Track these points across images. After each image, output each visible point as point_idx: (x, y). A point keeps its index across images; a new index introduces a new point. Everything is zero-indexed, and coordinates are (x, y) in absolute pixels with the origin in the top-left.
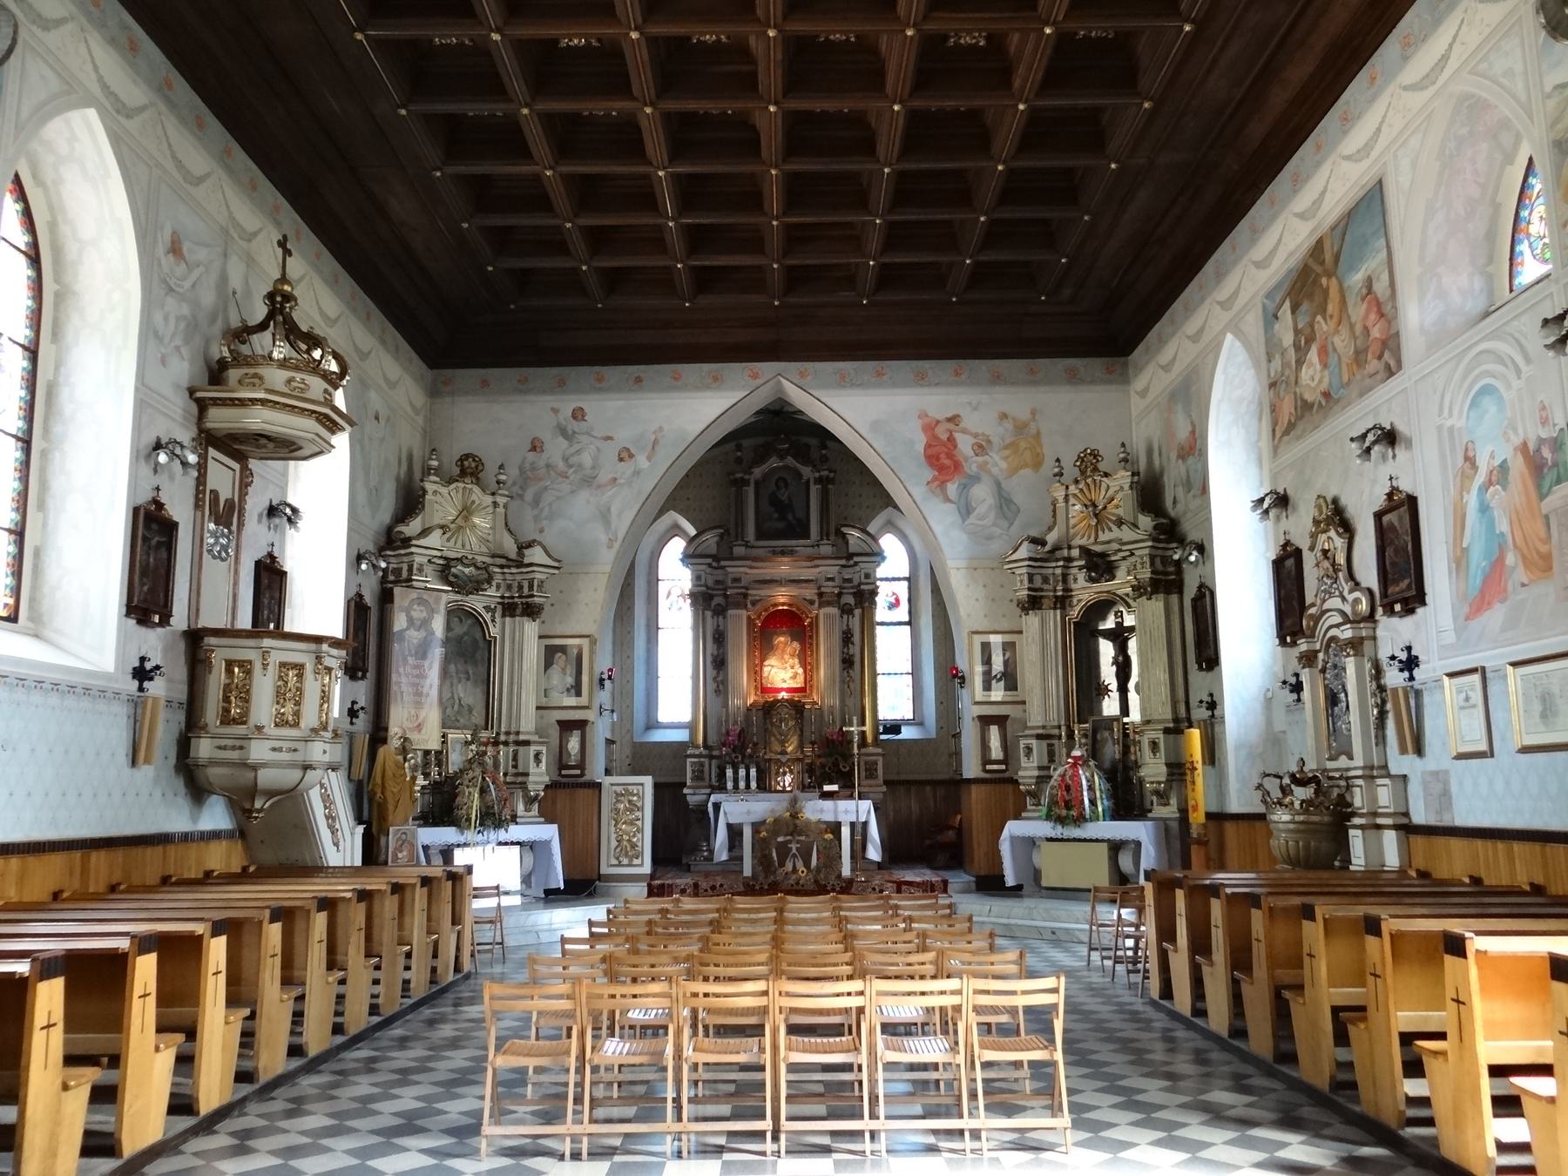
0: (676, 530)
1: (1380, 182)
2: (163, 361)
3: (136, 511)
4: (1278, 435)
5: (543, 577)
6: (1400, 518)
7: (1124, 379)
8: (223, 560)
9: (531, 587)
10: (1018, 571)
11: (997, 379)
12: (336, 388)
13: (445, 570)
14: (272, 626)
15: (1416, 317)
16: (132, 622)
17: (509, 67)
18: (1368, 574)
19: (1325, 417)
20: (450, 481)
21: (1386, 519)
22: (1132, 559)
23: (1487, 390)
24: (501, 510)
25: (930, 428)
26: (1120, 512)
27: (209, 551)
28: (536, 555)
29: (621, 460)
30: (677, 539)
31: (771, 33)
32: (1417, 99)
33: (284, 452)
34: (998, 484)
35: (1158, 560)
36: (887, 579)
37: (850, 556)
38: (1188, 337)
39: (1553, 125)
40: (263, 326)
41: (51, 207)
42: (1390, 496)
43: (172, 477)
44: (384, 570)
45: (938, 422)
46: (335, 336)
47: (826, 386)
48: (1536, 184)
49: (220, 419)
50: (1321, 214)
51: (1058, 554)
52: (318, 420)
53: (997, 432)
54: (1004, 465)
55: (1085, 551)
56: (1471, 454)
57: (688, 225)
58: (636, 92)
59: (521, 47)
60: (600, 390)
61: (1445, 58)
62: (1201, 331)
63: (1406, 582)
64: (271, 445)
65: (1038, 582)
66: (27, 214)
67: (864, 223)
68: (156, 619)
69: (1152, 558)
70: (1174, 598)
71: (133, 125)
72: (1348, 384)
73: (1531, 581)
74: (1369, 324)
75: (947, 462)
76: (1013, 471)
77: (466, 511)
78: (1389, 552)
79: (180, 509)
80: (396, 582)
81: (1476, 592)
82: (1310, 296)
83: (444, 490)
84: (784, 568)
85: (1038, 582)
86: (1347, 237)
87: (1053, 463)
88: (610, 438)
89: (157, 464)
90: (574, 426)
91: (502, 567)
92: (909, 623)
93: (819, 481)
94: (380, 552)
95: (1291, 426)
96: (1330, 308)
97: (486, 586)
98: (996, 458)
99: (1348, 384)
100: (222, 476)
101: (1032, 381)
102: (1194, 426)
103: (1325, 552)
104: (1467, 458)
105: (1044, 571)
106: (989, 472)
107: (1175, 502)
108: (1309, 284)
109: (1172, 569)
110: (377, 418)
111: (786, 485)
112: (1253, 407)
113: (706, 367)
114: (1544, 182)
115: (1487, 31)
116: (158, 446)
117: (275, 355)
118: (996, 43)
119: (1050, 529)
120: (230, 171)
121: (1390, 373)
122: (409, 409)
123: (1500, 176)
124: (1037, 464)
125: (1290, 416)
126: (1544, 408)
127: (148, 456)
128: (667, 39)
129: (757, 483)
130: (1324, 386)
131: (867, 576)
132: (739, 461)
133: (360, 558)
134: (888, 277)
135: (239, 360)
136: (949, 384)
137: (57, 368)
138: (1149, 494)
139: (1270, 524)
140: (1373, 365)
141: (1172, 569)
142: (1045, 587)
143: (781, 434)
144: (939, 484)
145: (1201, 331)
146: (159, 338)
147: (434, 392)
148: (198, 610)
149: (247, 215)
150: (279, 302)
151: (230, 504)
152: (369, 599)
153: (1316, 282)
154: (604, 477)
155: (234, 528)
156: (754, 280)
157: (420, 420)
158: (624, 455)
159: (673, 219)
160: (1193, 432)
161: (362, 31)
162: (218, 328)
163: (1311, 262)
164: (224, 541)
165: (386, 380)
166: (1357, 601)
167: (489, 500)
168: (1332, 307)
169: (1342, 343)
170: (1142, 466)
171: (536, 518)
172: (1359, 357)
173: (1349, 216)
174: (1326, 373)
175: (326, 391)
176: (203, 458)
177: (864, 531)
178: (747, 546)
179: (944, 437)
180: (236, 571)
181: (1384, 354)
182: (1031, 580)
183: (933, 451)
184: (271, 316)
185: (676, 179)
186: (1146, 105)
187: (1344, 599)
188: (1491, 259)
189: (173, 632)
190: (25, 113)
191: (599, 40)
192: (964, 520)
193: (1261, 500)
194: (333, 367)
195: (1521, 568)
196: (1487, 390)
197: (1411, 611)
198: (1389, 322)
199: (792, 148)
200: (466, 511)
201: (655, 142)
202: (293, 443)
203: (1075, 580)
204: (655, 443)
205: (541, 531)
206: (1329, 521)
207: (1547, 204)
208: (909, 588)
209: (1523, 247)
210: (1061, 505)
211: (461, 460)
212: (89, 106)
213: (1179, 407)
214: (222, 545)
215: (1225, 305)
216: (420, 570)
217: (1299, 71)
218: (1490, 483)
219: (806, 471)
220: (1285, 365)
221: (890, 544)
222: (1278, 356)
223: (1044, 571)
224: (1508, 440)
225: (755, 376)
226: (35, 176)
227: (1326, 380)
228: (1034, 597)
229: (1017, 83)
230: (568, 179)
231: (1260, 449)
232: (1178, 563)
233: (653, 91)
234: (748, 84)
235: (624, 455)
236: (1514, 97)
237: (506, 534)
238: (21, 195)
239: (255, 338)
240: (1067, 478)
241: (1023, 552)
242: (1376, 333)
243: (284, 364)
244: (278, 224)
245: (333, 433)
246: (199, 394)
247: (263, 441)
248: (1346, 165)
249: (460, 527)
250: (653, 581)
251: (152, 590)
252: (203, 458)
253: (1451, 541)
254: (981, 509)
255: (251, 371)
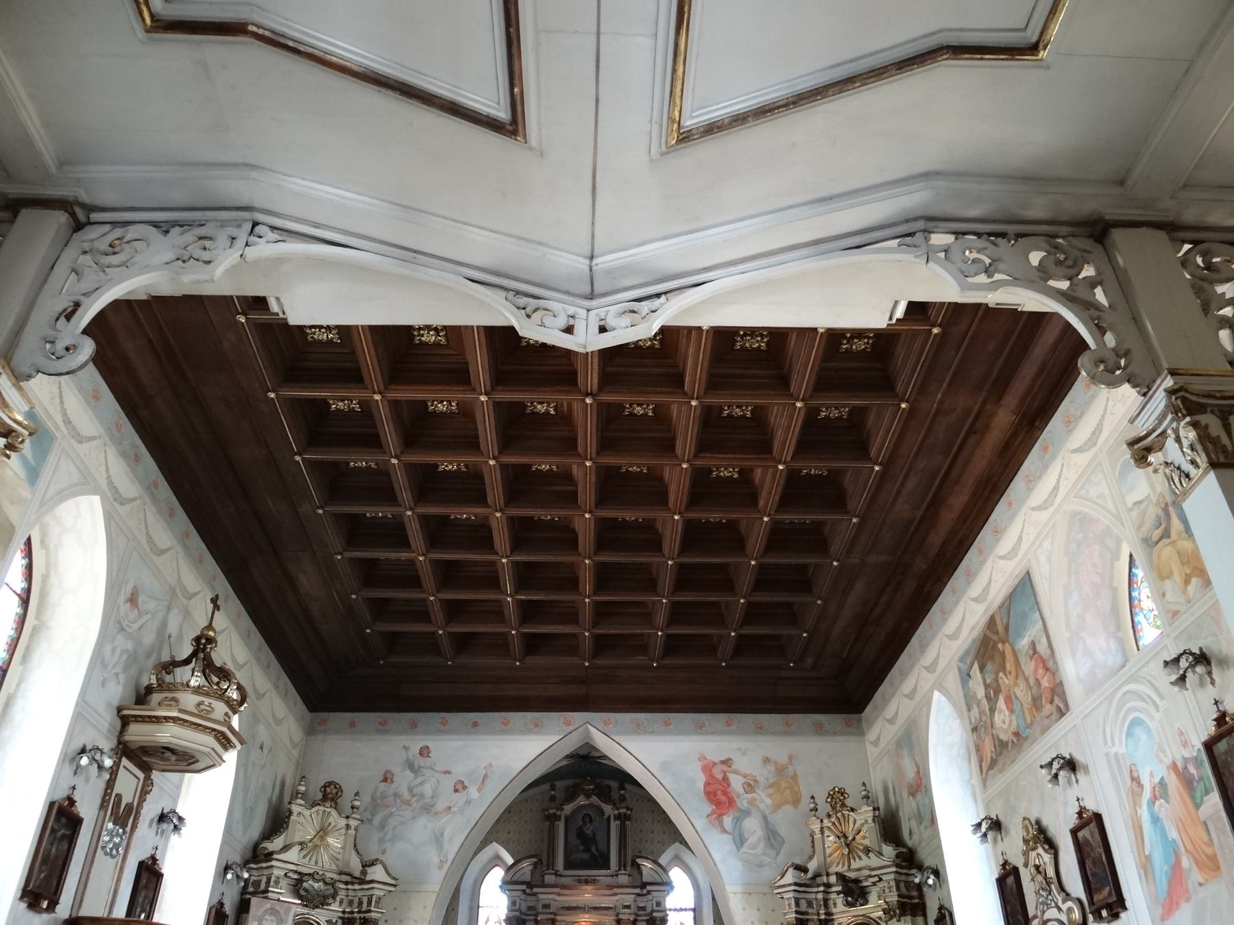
0: (496, 861)
1: (1028, 573)
2: (103, 684)
3: (52, 804)
4: (985, 770)
5: (381, 893)
6: (1092, 834)
7: (861, 733)
8: (113, 857)
9: (369, 903)
10: (786, 896)
11: (760, 730)
12: (235, 713)
13: (297, 888)
14: (143, 916)
15: (1072, 670)
16: (23, 905)
17: (401, 480)
18: (1075, 886)
19: (1019, 752)
20: (314, 805)
21: (1080, 834)
22: (881, 885)
23: (1136, 722)
24: (352, 832)
25: (708, 769)
26: (867, 842)
27: (103, 848)
28: (377, 873)
29: (456, 791)
30: (497, 869)
31: (588, 464)
32: (1044, 516)
33: (182, 766)
34: (765, 818)
35: (902, 885)
36: (675, 910)
37: (643, 885)
38: (905, 696)
39: (1139, 528)
40: (187, 662)
41: (48, 565)
42: (1080, 814)
43: (87, 780)
44: (246, 881)
45: (714, 764)
46: (240, 676)
47: (625, 733)
48: (1139, 573)
49: (138, 734)
50: (990, 597)
51: (819, 880)
52: (216, 738)
53: (763, 774)
54: (769, 801)
55: (841, 877)
56: (1135, 775)
57: (522, 601)
58: (490, 501)
59: (410, 468)
60: (444, 732)
61: (1056, 488)
62: (915, 690)
63: (1107, 889)
64: (173, 758)
65: (804, 907)
66: (29, 568)
67: (654, 602)
68: (45, 904)
69: (897, 882)
70: (920, 920)
71: (123, 510)
72: (1031, 724)
73: (1207, 880)
74: (1039, 677)
75: (723, 798)
76: (777, 807)
77: (323, 832)
78: (1088, 864)
79: (87, 809)
80: (254, 894)
81: (1165, 895)
82: (992, 658)
83: (307, 812)
84: (587, 895)
85: (804, 907)
86: (1012, 613)
87: (808, 800)
88: (449, 772)
89: (78, 766)
90: (421, 761)
91: (346, 883)
92: (694, 910)
93: (618, 817)
94: (245, 864)
95: (993, 763)
96: (1008, 666)
97: (331, 901)
98: (763, 795)
99: (1031, 724)
100: (127, 784)
101: (788, 732)
102: (918, 767)
103: (1037, 867)
104: (1133, 779)
105: (808, 896)
106: (757, 807)
107: (911, 833)
108: (990, 648)
109: (915, 893)
110: (261, 748)
111: (591, 821)
112: (963, 751)
113: (530, 715)
114: (1143, 570)
115: (1080, 470)
116: (83, 751)
117: (193, 683)
118: (745, 475)
119: (811, 858)
120: (185, 547)
121: (1062, 713)
122: (288, 743)
123: (1112, 568)
124: (796, 802)
125: (992, 754)
126: (1182, 733)
127: (73, 760)
128: (514, 466)
129: (567, 818)
130: (1013, 728)
131: (658, 904)
132: (553, 799)
133: (227, 868)
134: (673, 645)
135: (162, 686)
136: (722, 733)
137: (19, 684)
138: (889, 828)
139: (989, 846)
140: (1048, 708)
141: (915, 893)
142: (810, 911)
143: (588, 774)
144: (717, 816)
145: (915, 690)
146: (104, 665)
147: (310, 731)
148: (81, 901)
149: (191, 581)
150: (203, 643)
151: (129, 807)
152: (228, 908)
153: (994, 647)
154: (440, 805)
155: (128, 829)
156: (569, 645)
157: (295, 753)
158: (459, 787)
159: (511, 596)
160: (918, 772)
161: (300, 455)
162: (152, 661)
163: (988, 633)
164: (117, 840)
165: (274, 717)
166: (1070, 910)
167: (343, 822)
168: (1009, 666)
169: (1021, 692)
170: (881, 804)
171: (381, 841)
172: (1036, 703)
173: (1011, 598)
174: (1014, 717)
175: (226, 714)
176: (117, 765)
177: (656, 862)
178: (556, 875)
179: (720, 777)
180: (122, 868)
181: (1053, 700)
182: (797, 904)
183: (711, 788)
184: (194, 654)
185: (516, 565)
186: (854, 520)
187: (1059, 909)
188: (1119, 627)
189: (56, 920)
190: (49, 495)
191: (466, 466)
192: (738, 849)
193: (979, 825)
194: (235, 695)
195: (1195, 869)
196: (1136, 722)
197: (1116, 916)
198: (1054, 674)
199: (602, 544)
200: (323, 832)
201: (501, 538)
202: (193, 757)
203: (835, 904)
204: (486, 776)
205: (384, 852)
206: (1036, 839)
207: (1150, 586)
208: (695, 918)
209: (1139, 618)
210: (818, 836)
211: (325, 787)
212: (94, 493)
213: (905, 753)
214: (115, 844)
215: (930, 669)
216: (277, 883)
217: (958, 500)
218: (1155, 798)
219: (608, 809)
220: (981, 713)
221: (677, 875)
222: (975, 707)
223: (808, 896)
224: (1161, 762)
225: (568, 723)
226: (42, 542)
227: (1014, 723)
228: (801, 920)
229: (762, 503)
230: (435, 563)
231: (973, 786)
232: (919, 887)
233: (502, 501)
234: (570, 499)
235: (459, 787)
236: (1108, 511)
237: (354, 853)
238: (29, 554)
239: (178, 671)
240: (822, 812)
241: (790, 877)
242: (1045, 683)
243: (197, 690)
244: (213, 588)
245: (226, 749)
246: (125, 712)
247: (168, 754)
248: (1002, 563)
249: (316, 846)
250: (475, 908)
251: (48, 878)
252: (117, 765)
253: (1135, 850)
254: (752, 840)
255: (170, 695)
